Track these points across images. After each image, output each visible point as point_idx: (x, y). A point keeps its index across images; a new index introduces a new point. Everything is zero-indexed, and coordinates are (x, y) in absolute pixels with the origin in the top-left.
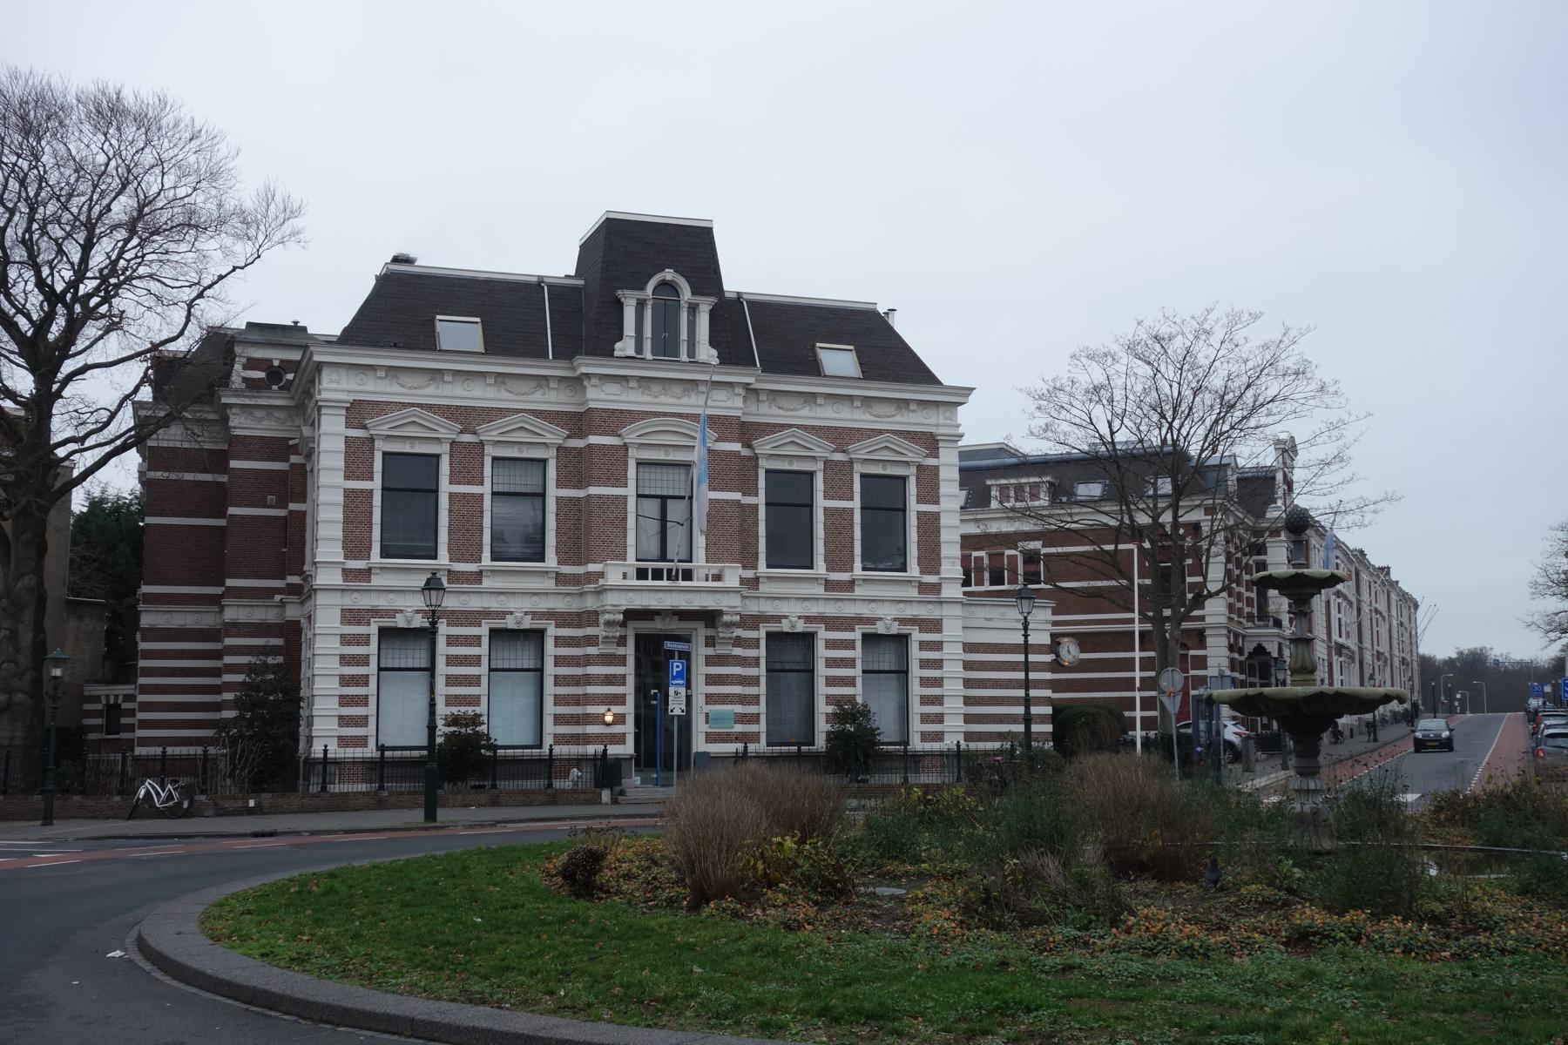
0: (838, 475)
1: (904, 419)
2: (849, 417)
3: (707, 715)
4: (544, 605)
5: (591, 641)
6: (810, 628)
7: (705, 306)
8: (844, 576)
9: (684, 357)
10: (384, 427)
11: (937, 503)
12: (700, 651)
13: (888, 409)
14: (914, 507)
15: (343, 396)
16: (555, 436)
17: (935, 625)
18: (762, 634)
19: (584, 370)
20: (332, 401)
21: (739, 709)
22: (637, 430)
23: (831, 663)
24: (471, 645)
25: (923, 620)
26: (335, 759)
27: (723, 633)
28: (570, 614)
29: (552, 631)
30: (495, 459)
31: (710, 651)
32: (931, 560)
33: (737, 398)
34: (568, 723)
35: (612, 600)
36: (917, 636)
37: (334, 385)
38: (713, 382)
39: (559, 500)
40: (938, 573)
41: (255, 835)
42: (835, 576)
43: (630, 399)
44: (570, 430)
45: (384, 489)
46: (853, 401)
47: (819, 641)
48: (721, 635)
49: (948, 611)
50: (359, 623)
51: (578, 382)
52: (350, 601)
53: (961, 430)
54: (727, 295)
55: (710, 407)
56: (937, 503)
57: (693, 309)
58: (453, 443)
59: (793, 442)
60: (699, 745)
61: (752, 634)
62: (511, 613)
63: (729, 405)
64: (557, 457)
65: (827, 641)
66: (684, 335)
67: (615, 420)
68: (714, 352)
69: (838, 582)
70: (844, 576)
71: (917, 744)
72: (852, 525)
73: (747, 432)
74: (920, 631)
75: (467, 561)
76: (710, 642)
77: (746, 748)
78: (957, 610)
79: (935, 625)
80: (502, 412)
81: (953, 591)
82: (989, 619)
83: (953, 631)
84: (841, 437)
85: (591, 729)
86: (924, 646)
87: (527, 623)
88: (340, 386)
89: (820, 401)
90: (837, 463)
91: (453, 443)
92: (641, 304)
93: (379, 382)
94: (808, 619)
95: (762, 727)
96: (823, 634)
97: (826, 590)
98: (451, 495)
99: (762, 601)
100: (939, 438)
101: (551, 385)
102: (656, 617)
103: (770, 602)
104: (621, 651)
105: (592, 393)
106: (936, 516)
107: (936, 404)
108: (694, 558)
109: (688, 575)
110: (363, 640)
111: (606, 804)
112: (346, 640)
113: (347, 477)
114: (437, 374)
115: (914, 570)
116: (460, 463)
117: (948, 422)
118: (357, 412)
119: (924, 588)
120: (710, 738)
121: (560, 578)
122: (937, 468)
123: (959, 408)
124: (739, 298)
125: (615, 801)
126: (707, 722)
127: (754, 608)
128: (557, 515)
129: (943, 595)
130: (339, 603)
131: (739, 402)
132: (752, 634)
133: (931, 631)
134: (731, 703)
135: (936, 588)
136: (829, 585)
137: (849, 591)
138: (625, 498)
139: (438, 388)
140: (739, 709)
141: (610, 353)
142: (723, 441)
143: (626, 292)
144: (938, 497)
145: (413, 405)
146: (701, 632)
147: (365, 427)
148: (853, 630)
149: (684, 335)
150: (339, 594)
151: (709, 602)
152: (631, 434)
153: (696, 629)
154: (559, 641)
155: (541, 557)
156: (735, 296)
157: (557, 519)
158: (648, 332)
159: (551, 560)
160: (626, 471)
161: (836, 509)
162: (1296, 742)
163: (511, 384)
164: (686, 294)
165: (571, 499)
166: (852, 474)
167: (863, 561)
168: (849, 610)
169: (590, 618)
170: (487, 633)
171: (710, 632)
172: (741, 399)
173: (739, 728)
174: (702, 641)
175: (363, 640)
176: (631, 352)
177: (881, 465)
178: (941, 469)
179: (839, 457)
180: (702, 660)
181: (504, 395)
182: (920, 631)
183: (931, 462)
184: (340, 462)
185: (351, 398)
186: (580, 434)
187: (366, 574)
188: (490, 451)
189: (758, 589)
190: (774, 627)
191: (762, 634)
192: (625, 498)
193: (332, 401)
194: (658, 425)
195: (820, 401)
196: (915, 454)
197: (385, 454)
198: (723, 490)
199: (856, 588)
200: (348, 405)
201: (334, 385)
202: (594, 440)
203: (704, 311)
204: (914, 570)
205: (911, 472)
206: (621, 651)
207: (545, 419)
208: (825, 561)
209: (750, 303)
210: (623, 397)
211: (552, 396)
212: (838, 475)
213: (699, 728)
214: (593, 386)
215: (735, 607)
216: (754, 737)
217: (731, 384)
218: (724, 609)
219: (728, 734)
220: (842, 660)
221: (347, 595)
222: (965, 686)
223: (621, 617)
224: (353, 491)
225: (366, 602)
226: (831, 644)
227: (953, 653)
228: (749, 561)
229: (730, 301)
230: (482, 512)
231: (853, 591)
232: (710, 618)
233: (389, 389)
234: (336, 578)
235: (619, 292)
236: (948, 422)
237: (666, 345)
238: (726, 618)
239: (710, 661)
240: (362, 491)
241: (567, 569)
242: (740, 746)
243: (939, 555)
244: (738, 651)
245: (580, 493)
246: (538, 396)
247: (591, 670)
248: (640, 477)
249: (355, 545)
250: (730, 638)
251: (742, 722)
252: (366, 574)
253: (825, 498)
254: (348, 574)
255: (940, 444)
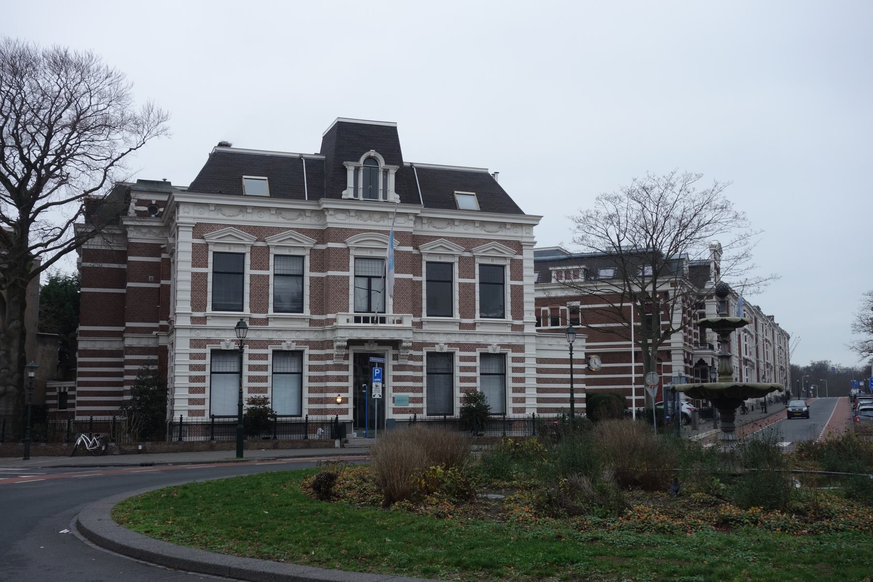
0: (467, 265)
1: (503, 234)
2: (473, 232)
3: (394, 398)
4: (303, 337)
5: (329, 357)
6: (451, 350)
7: (393, 170)
8: (470, 321)
9: (381, 199)
10: (214, 238)
11: (522, 280)
12: (390, 363)
13: (495, 228)
14: (509, 282)
15: (191, 221)
16: (309, 243)
17: (520, 348)
18: (424, 353)
19: (325, 206)
20: (185, 223)
21: (411, 395)
22: (354, 240)
23: (463, 369)
24: (262, 359)
25: (514, 345)
26: (187, 422)
27: (402, 353)
28: (317, 342)
29: (307, 351)
30: (275, 256)
31: (395, 363)
32: (518, 312)
33: (410, 222)
34: (316, 403)
35: (341, 334)
36: (510, 354)
37: (186, 215)
38: (397, 213)
39: (311, 278)
40: (522, 319)
41: (142, 465)
42: (465, 321)
43: (351, 222)
44: (317, 239)
45: (214, 272)
46: (475, 223)
47: (456, 357)
48: (401, 354)
49: (528, 340)
50: (200, 347)
51: (322, 213)
52: (195, 335)
53: (535, 240)
54: (405, 164)
55: (395, 227)
56: (522, 280)
57: (386, 172)
58: (252, 247)
59: (441, 246)
60: (389, 415)
61: (419, 353)
62: (285, 341)
63: (406, 225)
64: (310, 255)
65: (461, 357)
66: (381, 187)
67: (343, 234)
68: (398, 196)
69: (466, 324)
70: (470, 321)
71: (510, 415)
72: (474, 292)
73: (416, 240)
74: (512, 351)
75: (260, 313)
76: (396, 357)
77: (415, 416)
78: (533, 340)
79: (520, 348)
80: (280, 230)
81: (531, 329)
82: (551, 345)
83: (530, 352)
84: (468, 243)
85: (329, 406)
86: (515, 360)
87: (294, 347)
88: (190, 215)
89: (457, 223)
90: (466, 258)
91: (252, 247)
92: (357, 170)
93: (211, 213)
94: (450, 345)
95: (424, 405)
96: (458, 353)
97: (460, 329)
98: (251, 276)
99: (425, 335)
100: (523, 244)
101: (307, 215)
102: (365, 344)
103: (429, 335)
104: (346, 363)
105: (329, 219)
106: (521, 288)
107: (521, 225)
108: (386, 311)
109: (383, 320)
110: (202, 356)
111: (337, 448)
112: (193, 356)
113: (193, 266)
114: (243, 208)
115: (509, 317)
116: (256, 258)
117: (528, 235)
118: (199, 229)
119: (514, 327)
120: (395, 411)
121: (312, 322)
122: (521, 261)
123: (534, 227)
124: (411, 166)
125: (342, 446)
126: (394, 402)
127: (420, 338)
128: (310, 287)
129: (525, 332)
130: (189, 336)
131: (411, 224)
132: (419, 353)
133: (518, 351)
134: (407, 391)
135: (521, 328)
136: (462, 326)
137: (473, 329)
138: (348, 277)
139: (244, 216)
140: (411, 395)
141: (339, 197)
142: (403, 245)
143: (348, 162)
144: (522, 277)
145: (230, 225)
146: (390, 352)
147: (203, 238)
148: (475, 351)
149: (381, 187)
150: (189, 331)
151: (395, 335)
152: (351, 242)
153: (387, 350)
154: (311, 357)
155: (301, 310)
156: (409, 165)
157: (310, 289)
158: (361, 185)
159: (307, 312)
160: (349, 262)
161: (466, 284)
162: (721, 413)
163: (285, 214)
164: (382, 164)
165: (318, 278)
166: (474, 264)
167: (480, 312)
168: (473, 340)
169: (329, 344)
170: (271, 352)
171: (395, 352)
172: (412, 222)
173: (411, 405)
174: (391, 357)
175: (202, 356)
176: (352, 196)
177: (490, 259)
178: (524, 261)
179: (467, 254)
180: (391, 368)
181: (281, 220)
182: (512, 351)
183: (519, 257)
184: (189, 257)
185: (196, 222)
186: (323, 242)
187: (204, 320)
188: (273, 251)
189: (422, 328)
190: (431, 349)
191: (424, 353)
192: (348, 277)
193: (185, 223)
194: (366, 237)
195: (457, 223)
196: (509, 253)
197: (214, 253)
198: (402, 273)
199: (477, 328)
200: (194, 226)
201: (186, 215)
202: (331, 245)
203: (392, 173)
204: (509, 317)
205: (507, 263)
206: (346, 363)
207: (303, 233)
208: (460, 312)
209: (418, 169)
210: (347, 221)
211: (307, 220)
212: (467, 265)
213: (389, 405)
214: (330, 215)
215: (409, 338)
216: (420, 411)
217: (407, 214)
218: (403, 339)
219: (405, 409)
220: (469, 367)
221: (193, 331)
222: (537, 382)
223: (346, 344)
224: (197, 273)
225: (204, 335)
226: (463, 359)
227: (530, 363)
228: (417, 313)
229: (407, 168)
230: (268, 285)
231: (475, 329)
232: (395, 344)
233: (217, 217)
234: (187, 322)
235: (345, 163)
236: (528, 235)
237: (371, 192)
238: (404, 344)
239: (395, 368)
240: (202, 274)
241: (316, 317)
242: (412, 416)
243: (523, 309)
244: (411, 363)
245: (323, 275)
246: (299, 220)
247: (329, 373)
248: (357, 265)
249: (198, 303)
250: (406, 356)
251: (413, 402)
252: (204, 320)
253: (459, 277)
254: (194, 319)
255: (524, 248)
